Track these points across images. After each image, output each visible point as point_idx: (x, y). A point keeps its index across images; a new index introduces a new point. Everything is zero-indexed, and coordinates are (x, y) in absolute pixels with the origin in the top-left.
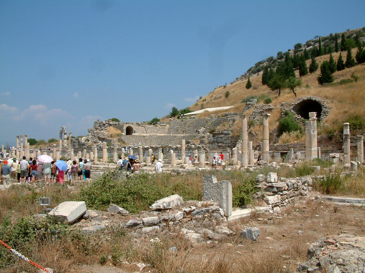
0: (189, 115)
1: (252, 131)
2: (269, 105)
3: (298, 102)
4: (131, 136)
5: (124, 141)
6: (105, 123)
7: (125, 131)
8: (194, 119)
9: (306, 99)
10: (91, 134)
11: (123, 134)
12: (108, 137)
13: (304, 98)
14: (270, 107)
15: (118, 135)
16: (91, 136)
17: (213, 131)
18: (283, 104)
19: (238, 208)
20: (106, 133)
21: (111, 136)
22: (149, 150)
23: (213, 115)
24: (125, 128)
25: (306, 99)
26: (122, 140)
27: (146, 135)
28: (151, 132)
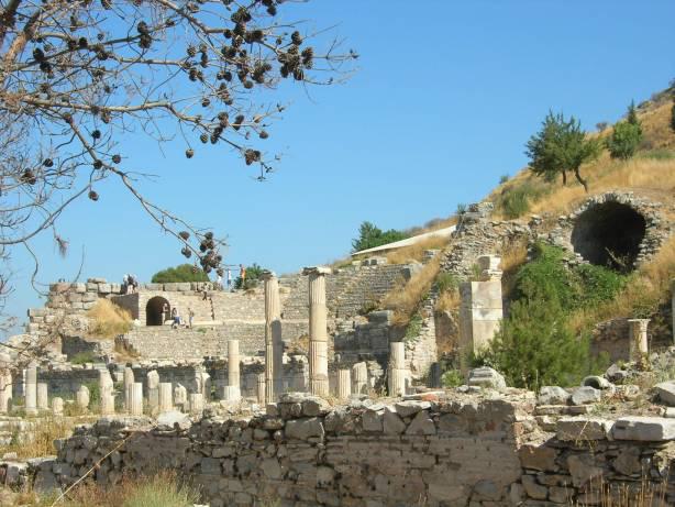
0: (396, 249)
1: (444, 307)
2: (516, 221)
3: (580, 211)
4: (158, 328)
5: (131, 346)
6: (84, 290)
7: (143, 314)
8: (374, 267)
9: (600, 200)
10: (36, 325)
11: (137, 322)
12: (90, 333)
13: (596, 198)
14: (517, 229)
15: (117, 328)
16: (38, 333)
17: (373, 309)
18: (533, 218)
19: (128, 486)
20: (85, 321)
21: (98, 331)
22: (150, 374)
23: (434, 251)
24: (142, 304)
25: (601, 202)
26: (125, 342)
27: (212, 322)
28: (228, 314)
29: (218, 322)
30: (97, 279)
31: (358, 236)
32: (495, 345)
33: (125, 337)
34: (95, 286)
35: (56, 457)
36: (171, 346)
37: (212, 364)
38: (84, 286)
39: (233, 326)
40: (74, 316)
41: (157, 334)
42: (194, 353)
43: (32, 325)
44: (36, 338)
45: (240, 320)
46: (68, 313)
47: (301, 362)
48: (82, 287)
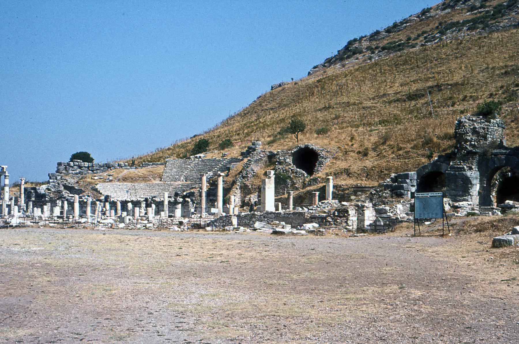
16: (53, 184)
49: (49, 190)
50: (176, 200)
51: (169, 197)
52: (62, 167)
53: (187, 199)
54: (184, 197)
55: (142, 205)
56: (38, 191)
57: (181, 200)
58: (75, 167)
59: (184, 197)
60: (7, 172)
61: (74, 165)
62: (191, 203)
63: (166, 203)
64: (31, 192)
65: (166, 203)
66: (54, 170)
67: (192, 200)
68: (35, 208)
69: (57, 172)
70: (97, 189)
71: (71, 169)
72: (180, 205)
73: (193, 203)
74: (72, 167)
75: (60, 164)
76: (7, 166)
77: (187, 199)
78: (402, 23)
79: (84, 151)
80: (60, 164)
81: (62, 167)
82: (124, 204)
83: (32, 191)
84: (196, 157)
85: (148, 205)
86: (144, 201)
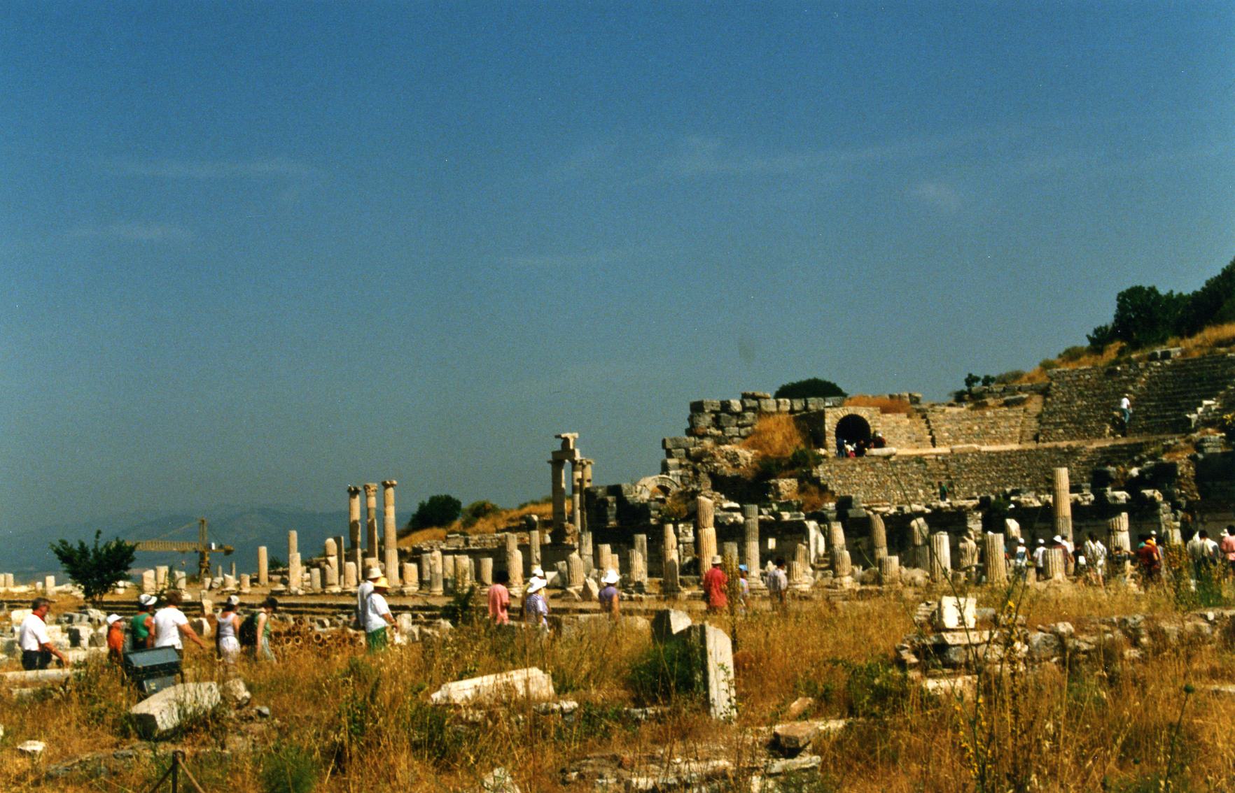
8: (1168, 362)
16: (680, 472)
26: (816, 481)
29: (943, 450)
30: (758, 394)
31: (1107, 316)
32: (309, 784)
33: (815, 474)
34: (755, 403)
35: (576, 705)
36: (882, 485)
37: (465, 607)
38: (738, 403)
39: (966, 455)
40: (727, 447)
41: (858, 469)
42: (917, 494)
43: (670, 461)
44: (677, 480)
45: (976, 446)
46: (719, 441)
47: (1153, 499)
48: (736, 405)
49: (665, 490)
50: (1100, 496)
51: (1073, 489)
52: (705, 421)
53: (1148, 492)
54: (1133, 486)
55: (970, 525)
56: (629, 497)
57: (1122, 496)
58: (749, 415)
59: (1133, 486)
60: (577, 452)
61: (745, 409)
62: (1165, 506)
63: (1066, 510)
64: (605, 502)
65: (1066, 510)
66: (677, 429)
67: (1168, 497)
68: (159, 644)
69: (690, 432)
70: (818, 479)
71: (734, 421)
72: (1125, 515)
73: (1175, 507)
74: (739, 415)
75: (697, 408)
76: (576, 435)
77: (1148, 492)
78: (931, 549)
79: (811, 377)
80: (697, 408)
81: (705, 421)
82: (899, 527)
83: (610, 499)
84: (1153, 357)
85: (993, 522)
86: (977, 508)
